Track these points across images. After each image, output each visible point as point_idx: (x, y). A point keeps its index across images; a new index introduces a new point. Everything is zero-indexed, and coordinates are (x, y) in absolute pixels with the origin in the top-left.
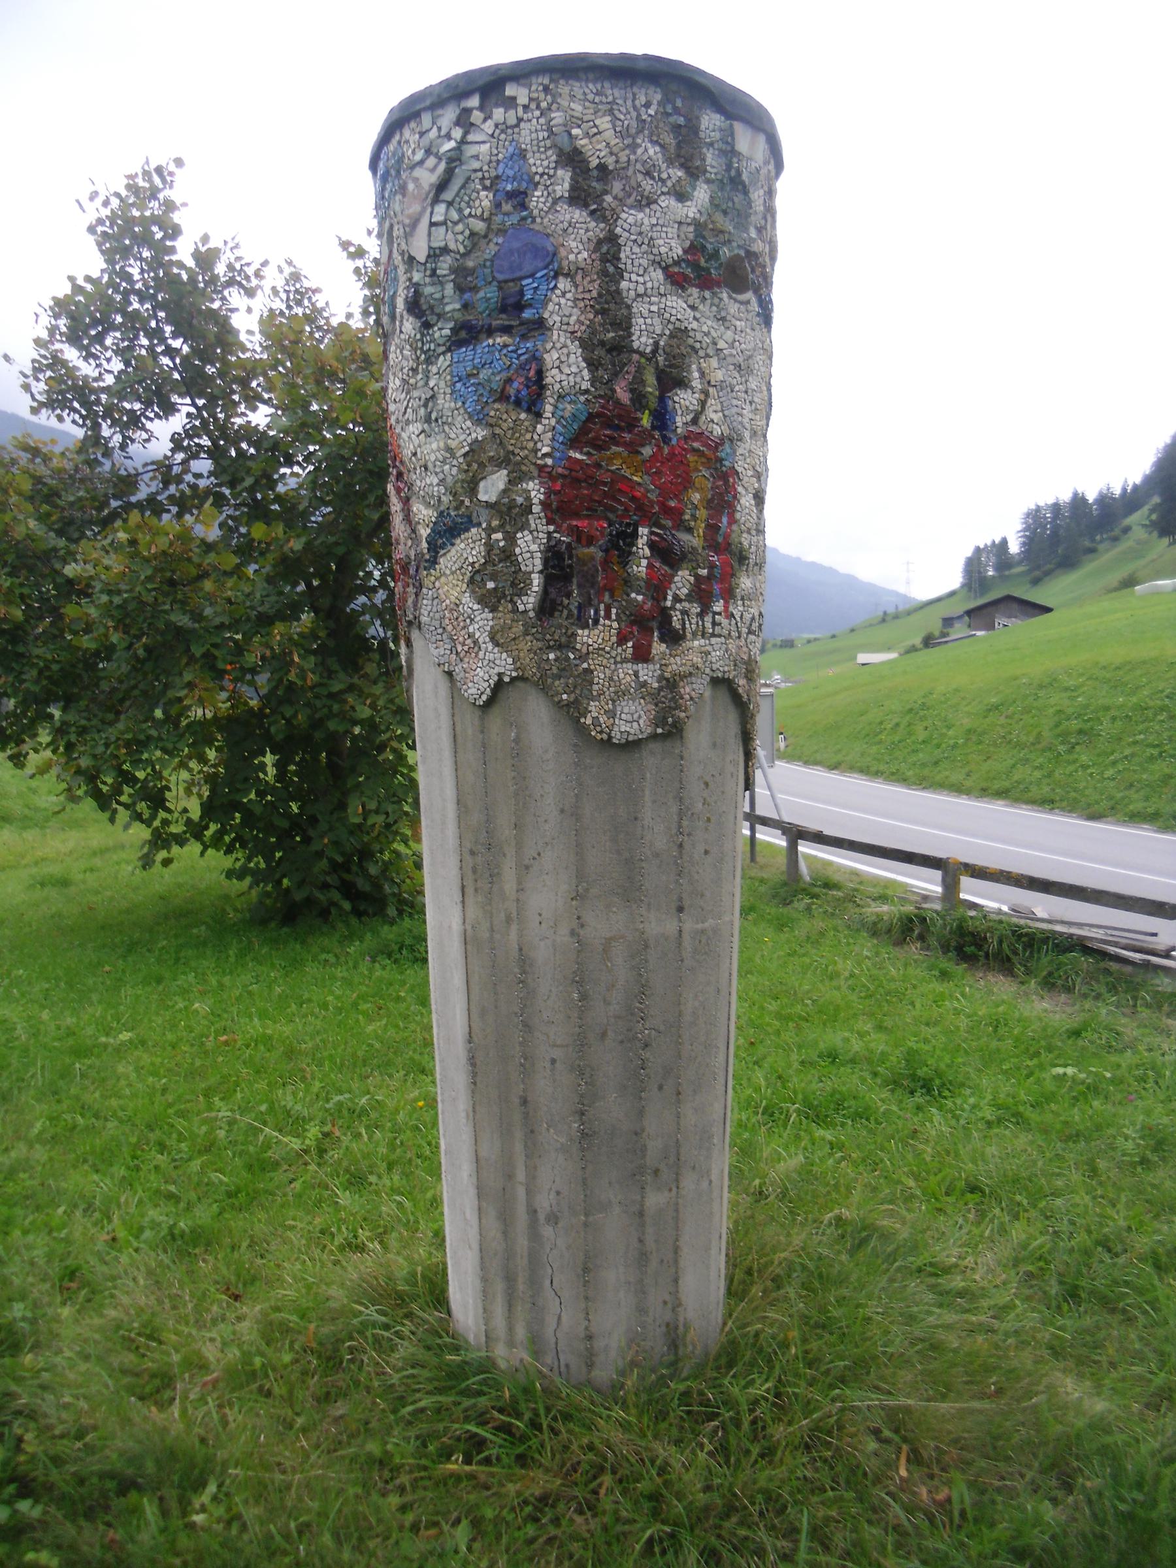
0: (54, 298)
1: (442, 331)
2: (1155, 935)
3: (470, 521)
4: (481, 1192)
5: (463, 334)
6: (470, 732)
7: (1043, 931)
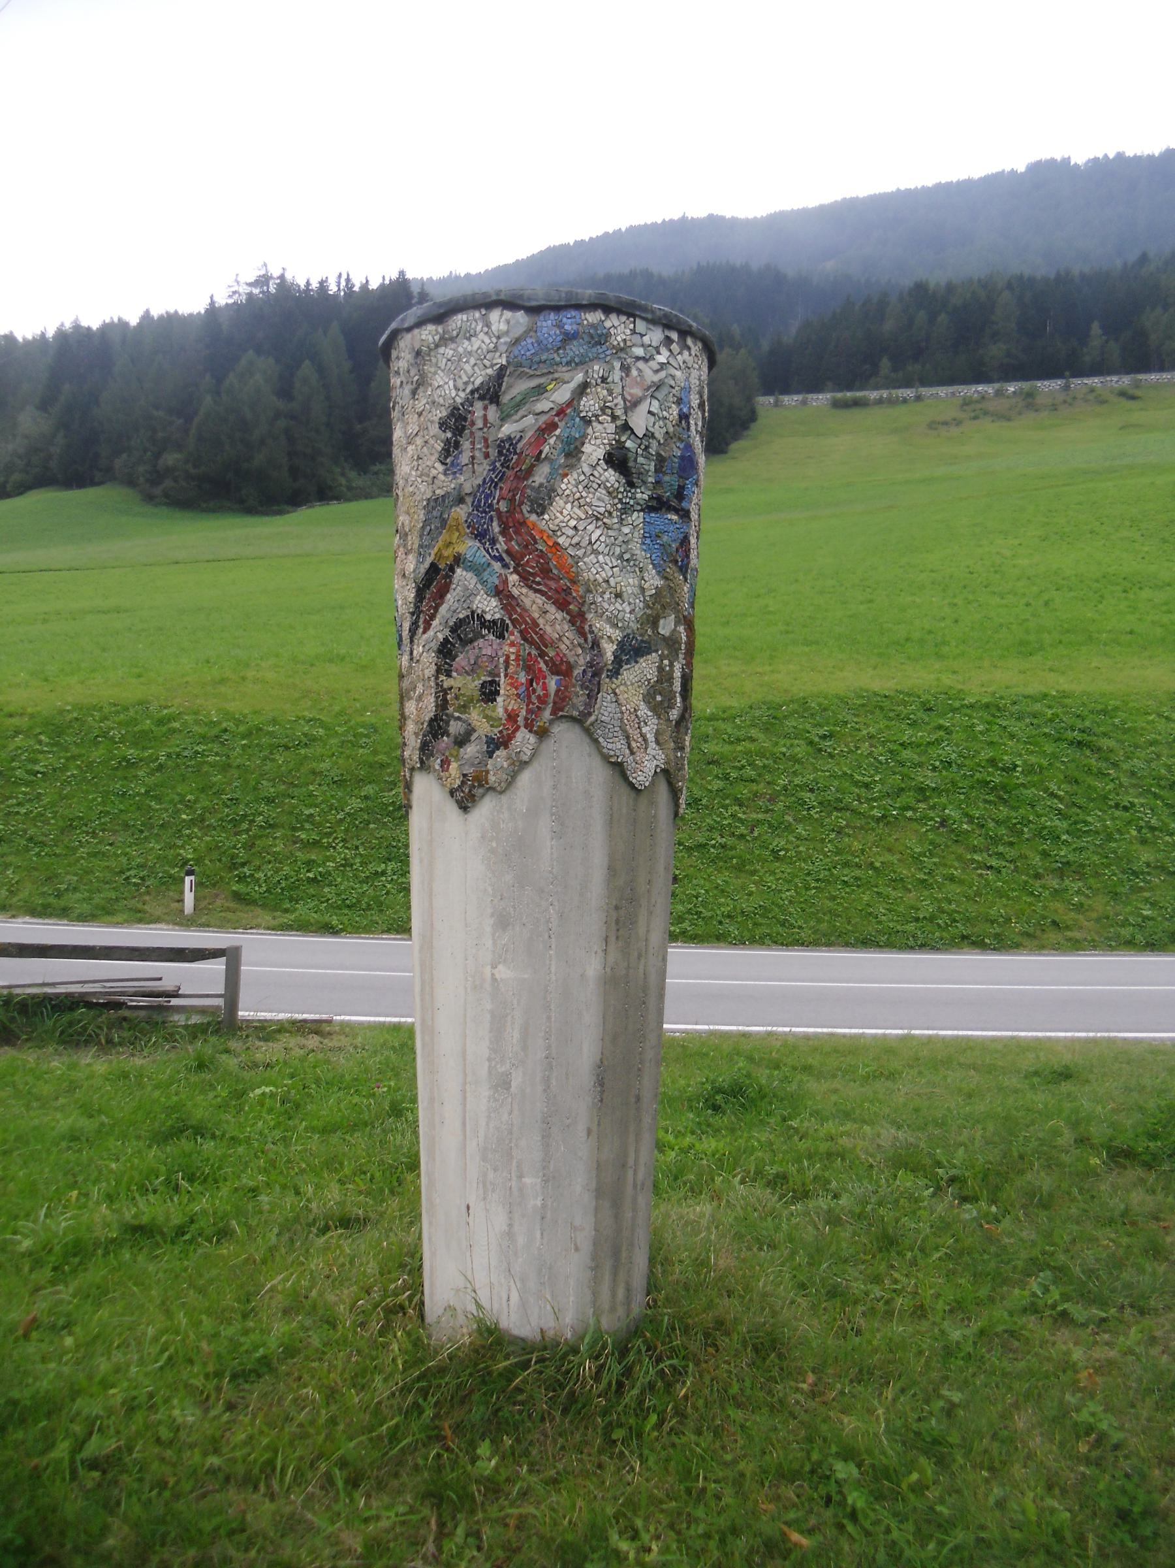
0: (402, 273)
1: (642, 495)
2: (160, 979)
3: (650, 648)
4: (599, 1193)
5: (654, 503)
6: (624, 811)
7: (34, 996)
